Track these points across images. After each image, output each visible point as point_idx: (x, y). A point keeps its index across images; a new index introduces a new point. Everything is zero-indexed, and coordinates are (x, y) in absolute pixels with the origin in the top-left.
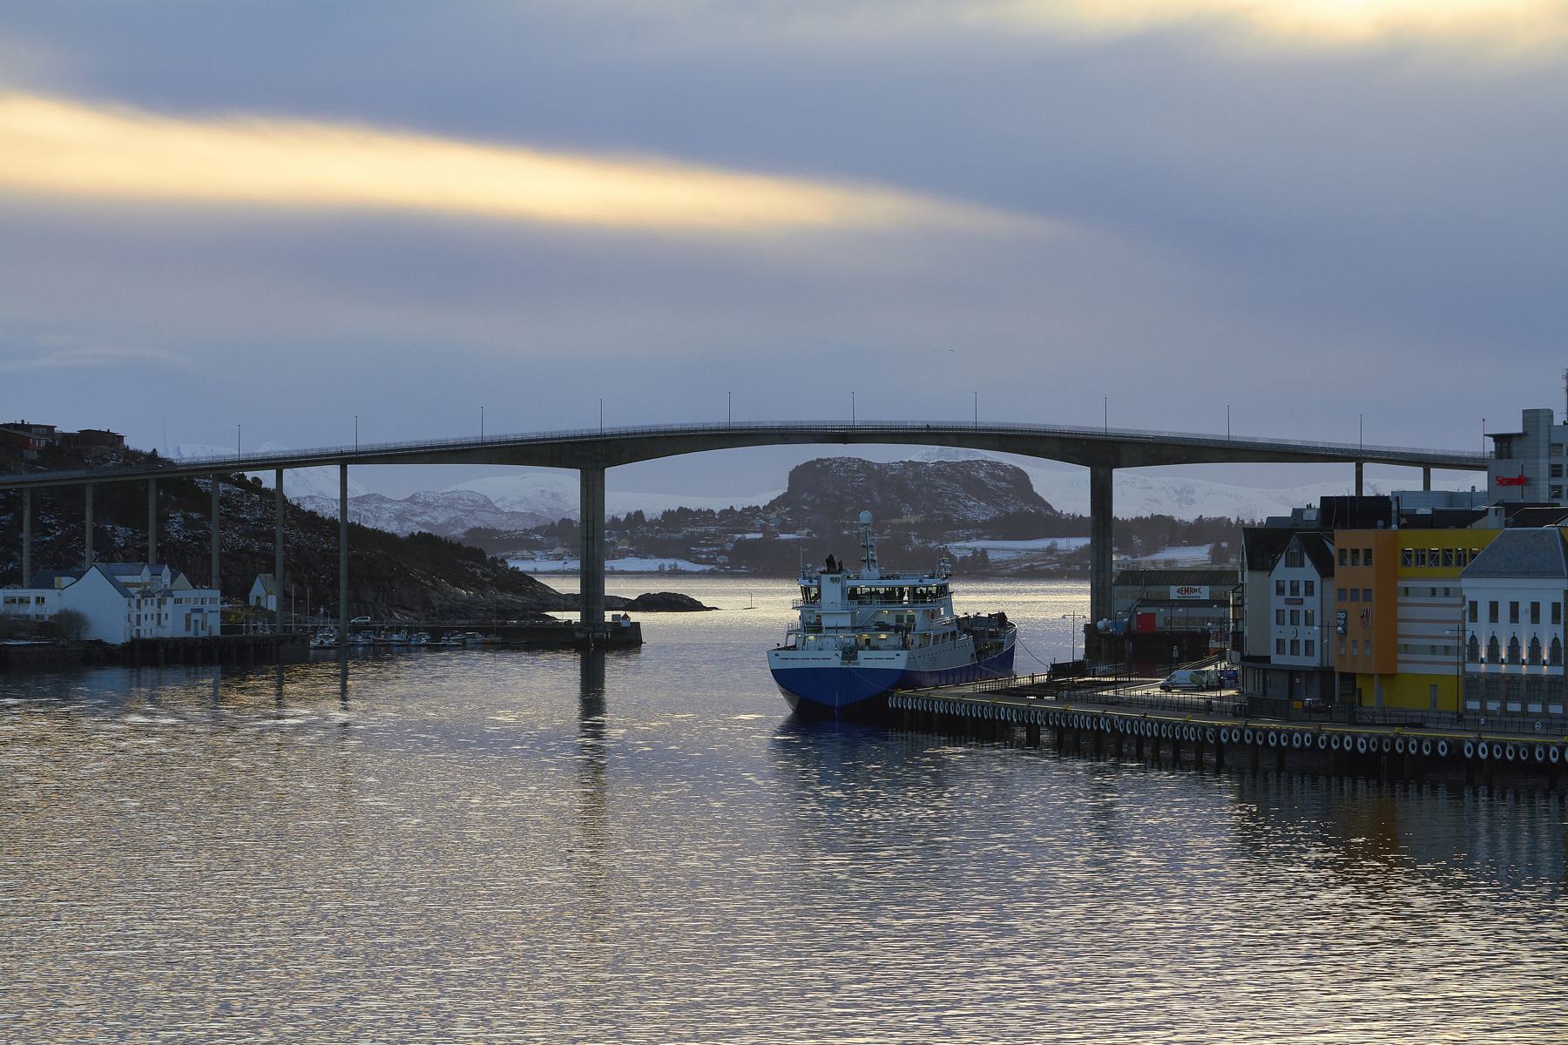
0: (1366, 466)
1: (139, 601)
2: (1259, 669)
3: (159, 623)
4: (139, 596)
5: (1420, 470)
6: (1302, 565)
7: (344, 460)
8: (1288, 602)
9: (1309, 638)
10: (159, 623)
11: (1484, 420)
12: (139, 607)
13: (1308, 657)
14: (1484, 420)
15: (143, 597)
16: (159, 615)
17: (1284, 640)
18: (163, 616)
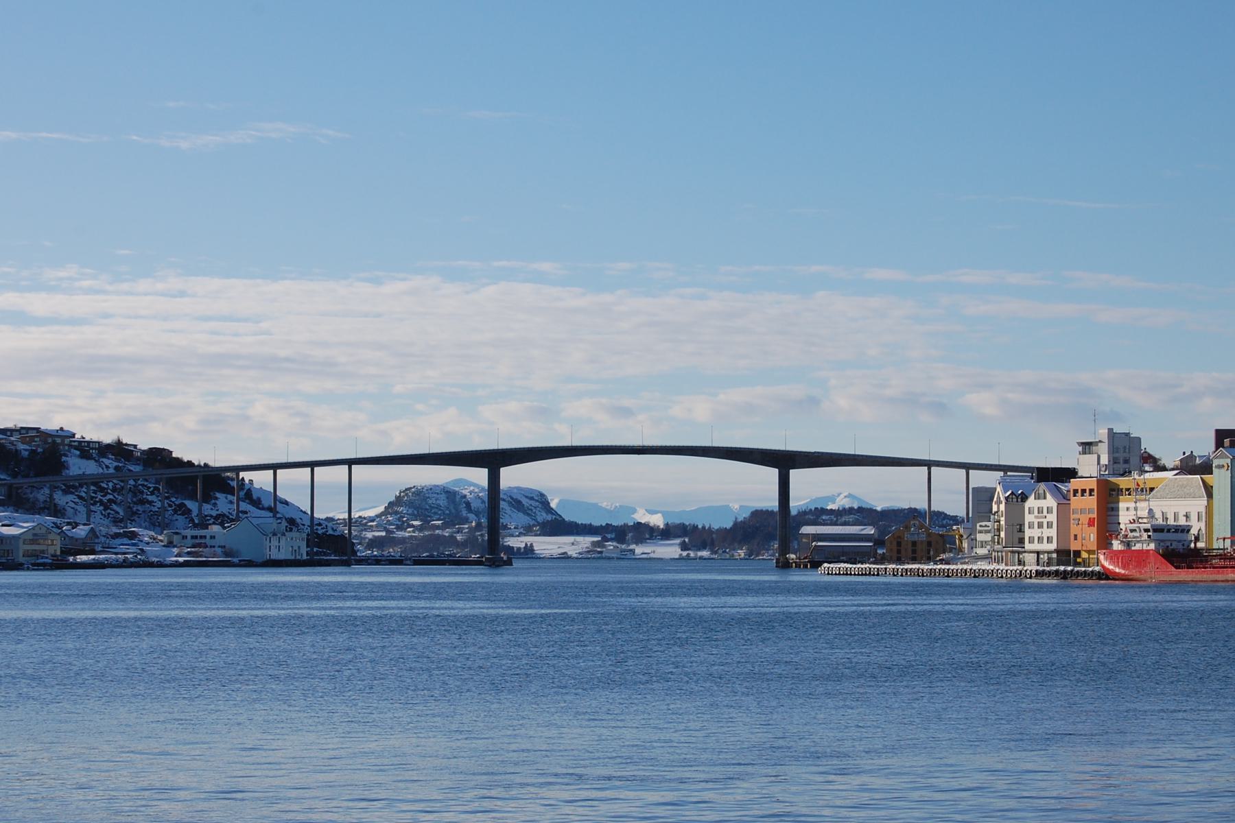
0: (316, 469)
1: (270, 538)
2: (851, 574)
3: (279, 550)
4: (270, 535)
5: (271, 472)
6: (1045, 498)
7: (275, 467)
8: (1036, 517)
9: (1049, 535)
10: (279, 550)
11: (999, 444)
12: (270, 541)
13: (1030, 545)
14: (999, 444)
15: (273, 535)
16: (279, 547)
17: (1052, 537)
18: (281, 547)
